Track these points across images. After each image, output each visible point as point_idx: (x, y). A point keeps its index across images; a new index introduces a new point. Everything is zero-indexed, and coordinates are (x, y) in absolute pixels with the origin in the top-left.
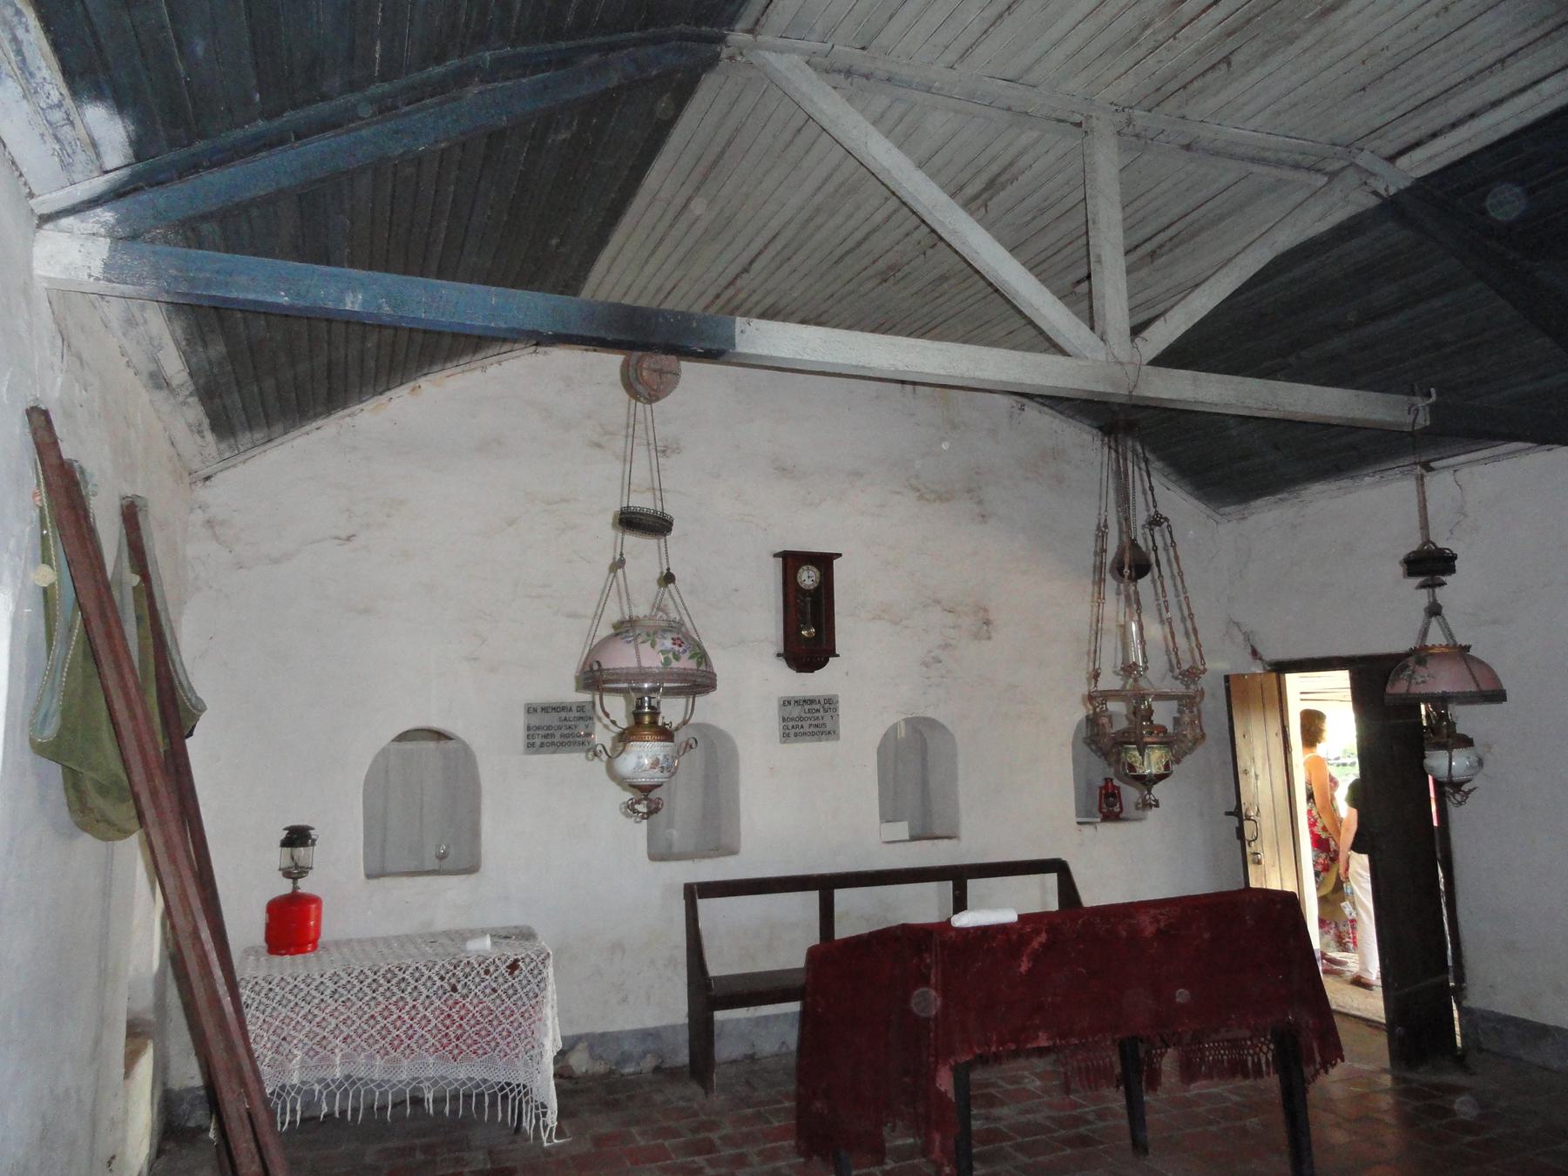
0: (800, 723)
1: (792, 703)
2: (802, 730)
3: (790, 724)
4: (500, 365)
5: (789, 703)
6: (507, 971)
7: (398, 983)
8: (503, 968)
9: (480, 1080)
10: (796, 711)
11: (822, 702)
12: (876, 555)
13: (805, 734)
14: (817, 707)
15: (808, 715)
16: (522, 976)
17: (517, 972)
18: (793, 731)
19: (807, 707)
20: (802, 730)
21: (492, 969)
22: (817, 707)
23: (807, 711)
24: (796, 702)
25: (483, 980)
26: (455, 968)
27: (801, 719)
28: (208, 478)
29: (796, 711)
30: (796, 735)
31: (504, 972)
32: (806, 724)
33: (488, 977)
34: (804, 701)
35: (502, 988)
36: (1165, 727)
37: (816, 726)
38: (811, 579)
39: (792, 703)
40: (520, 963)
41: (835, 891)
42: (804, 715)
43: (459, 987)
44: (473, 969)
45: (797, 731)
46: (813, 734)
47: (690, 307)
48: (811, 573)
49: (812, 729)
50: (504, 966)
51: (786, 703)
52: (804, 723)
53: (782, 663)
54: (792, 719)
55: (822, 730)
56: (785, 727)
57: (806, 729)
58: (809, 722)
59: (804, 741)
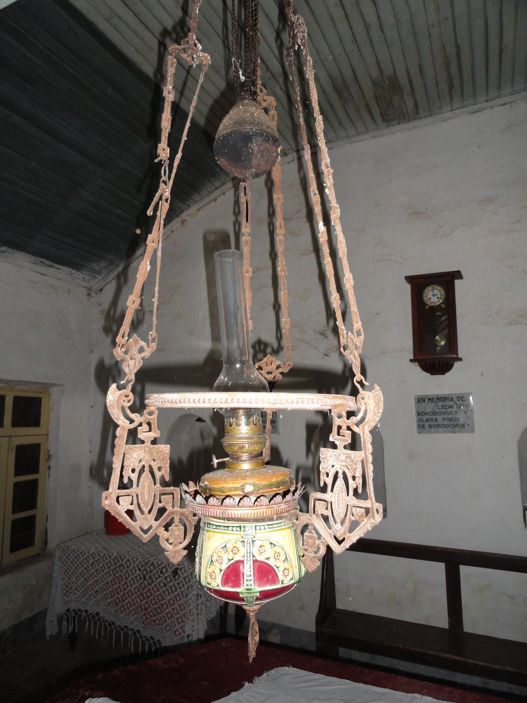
0: (434, 417)
1: (426, 400)
2: (436, 423)
3: (425, 418)
4: (224, 195)
5: (423, 400)
6: (172, 575)
7: (119, 566)
8: (169, 573)
9: (157, 640)
10: (429, 407)
11: (455, 399)
12: (511, 267)
13: (439, 426)
14: (451, 403)
15: (442, 410)
16: (180, 580)
17: (177, 577)
18: (427, 424)
19: (440, 404)
20: (436, 423)
21: (164, 570)
22: (451, 403)
23: (440, 407)
24: (429, 399)
25: (159, 577)
26: (146, 565)
27: (434, 413)
28: (101, 290)
29: (429, 407)
30: (430, 426)
31: (170, 574)
32: (440, 418)
33: (162, 575)
34: (438, 399)
35: (169, 585)
36: (357, 498)
37: (431, 420)
38: (436, 297)
39: (426, 400)
40: (178, 571)
41: (444, 564)
42: (437, 411)
43: (147, 577)
44: (155, 568)
45: (432, 423)
46: (446, 426)
47: (185, 98)
48: (436, 292)
49: (446, 422)
50: (171, 571)
51: (420, 400)
52: (438, 417)
53: (416, 368)
54: (427, 414)
55: (456, 423)
56: (419, 420)
57: (440, 422)
58: (443, 416)
59: (438, 432)
